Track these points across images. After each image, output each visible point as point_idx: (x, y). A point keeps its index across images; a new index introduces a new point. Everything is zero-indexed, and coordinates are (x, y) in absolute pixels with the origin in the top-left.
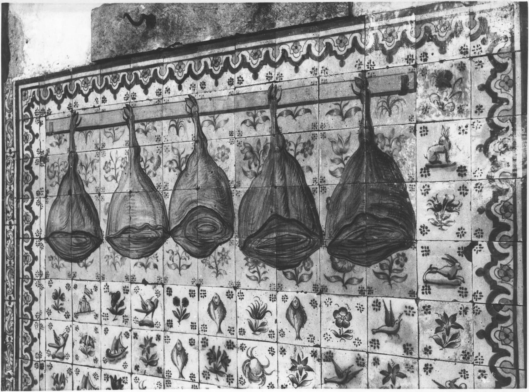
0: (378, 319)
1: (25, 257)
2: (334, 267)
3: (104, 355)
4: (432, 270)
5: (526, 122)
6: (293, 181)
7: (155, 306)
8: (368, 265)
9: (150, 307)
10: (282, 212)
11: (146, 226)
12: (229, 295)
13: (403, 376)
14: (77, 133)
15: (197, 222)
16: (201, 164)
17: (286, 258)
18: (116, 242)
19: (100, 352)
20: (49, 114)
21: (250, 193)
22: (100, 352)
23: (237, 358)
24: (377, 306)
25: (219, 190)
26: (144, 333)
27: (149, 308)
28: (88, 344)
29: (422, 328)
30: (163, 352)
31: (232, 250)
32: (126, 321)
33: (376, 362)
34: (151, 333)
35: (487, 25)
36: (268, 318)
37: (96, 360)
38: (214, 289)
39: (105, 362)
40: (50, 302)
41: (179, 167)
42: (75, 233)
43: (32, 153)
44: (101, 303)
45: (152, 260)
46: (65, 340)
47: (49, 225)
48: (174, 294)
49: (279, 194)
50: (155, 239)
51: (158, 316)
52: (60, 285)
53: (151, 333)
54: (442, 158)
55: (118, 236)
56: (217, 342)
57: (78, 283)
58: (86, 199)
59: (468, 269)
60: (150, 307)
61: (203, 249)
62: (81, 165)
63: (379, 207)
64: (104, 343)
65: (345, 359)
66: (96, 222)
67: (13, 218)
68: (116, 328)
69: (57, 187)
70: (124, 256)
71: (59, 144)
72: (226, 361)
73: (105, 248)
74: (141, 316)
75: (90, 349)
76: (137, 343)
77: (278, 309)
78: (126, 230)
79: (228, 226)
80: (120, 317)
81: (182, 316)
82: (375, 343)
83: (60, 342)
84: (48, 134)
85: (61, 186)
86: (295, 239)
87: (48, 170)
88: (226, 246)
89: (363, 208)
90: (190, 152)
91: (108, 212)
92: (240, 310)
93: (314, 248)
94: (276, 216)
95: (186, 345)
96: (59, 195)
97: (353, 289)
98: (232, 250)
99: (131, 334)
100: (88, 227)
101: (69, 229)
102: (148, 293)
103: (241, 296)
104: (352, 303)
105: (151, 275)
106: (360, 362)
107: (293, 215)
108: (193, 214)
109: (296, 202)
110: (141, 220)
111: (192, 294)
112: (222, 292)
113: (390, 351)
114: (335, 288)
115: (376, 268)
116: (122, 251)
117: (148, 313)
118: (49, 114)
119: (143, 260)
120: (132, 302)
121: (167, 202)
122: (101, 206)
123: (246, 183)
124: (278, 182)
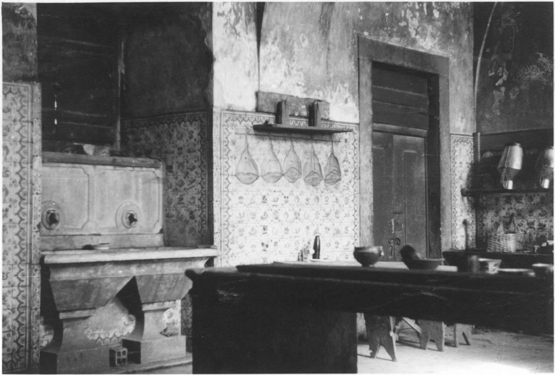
0: (334, 199)
1: (225, 183)
2: (325, 186)
3: (260, 218)
4: (344, 186)
5: (3, 321)
6: (316, 162)
7: (278, 199)
8: (332, 185)
9: (276, 200)
10: (313, 170)
11: (276, 172)
12: (300, 194)
13: (324, 217)
14: (248, 136)
15: (292, 172)
16: (292, 153)
17: (314, 184)
18: (265, 177)
19: (258, 217)
20: (236, 126)
21: (306, 163)
22: (258, 217)
23: (302, 213)
24: (334, 195)
25: (298, 162)
26: (275, 208)
27: (276, 200)
28: (254, 215)
29: (342, 201)
30: (281, 216)
31: (301, 181)
32: (268, 205)
33: (334, 210)
34: (276, 209)
35: (164, 237)
36: (310, 201)
37: (257, 221)
38: (296, 193)
39: (260, 220)
40: (238, 200)
41: (286, 153)
42: (248, 174)
43: (19, 333)
44: (259, 199)
45: (277, 183)
46: (244, 214)
47: (237, 170)
48: (284, 195)
49: (313, 164)
50: (278, 177)
51: (279, 203)
52: (241, 194)
53: (276, 209)
54: (346, 159)
55: (265, 175)
56: (297, 209)
57: (250, 193)
58: (252, 161)
59: (350, 186)
60: (276, 200)
61: (293, 180)
62: (250, 148)
63: (335, 170)
64: (261, 214)
65: (327, 210)
66: (256, 169)
67: (218, 166)
68: (264, 208)
69: (240, 156)
70: (268, 182)
71: (240, 138)
72: (299, 215)
73: (260, 179)
74: (274, 203)
75: (254, 216)
76: (271, 212)
77: (313, 198)
78: (268, 173)
79: (300, 173)
80: (266, 204)
81: (287, 202)
82: (334, 205)
83: (241, 216)
84: (236, 134)
85: (242, 155)
86: (317, 178)
87: (236, 148)
88: (300, 179)
89: (331, 170)
90: (289, 149)
91: (261, 166)
92: (303, 199)
93: (321, 180)
94: (313, 171)
95: (288, 211)
96: (241, 159)
97: (329, 191)
98: (301, 181)
99: (270, 210)
100: (254, 172)
101: (246, 172)
102: (276, 195)
103: (304, 194)
104: (329, 195)
105: (276, 189)
106: (331, 210)
107: (316, 171)
108: (290, 169)
109: (317, 167)
110: (273, 170)
111: (290, 194)
112: (298, 194)
113: (337, 207)
114: (325, 191)
115: (334, 186)
116: (267, 181)
117: (275, 202)
118: (236, 126)
119: (274, 184)
120: (270, 199)
121: (282, 164)
122: (258, 164)
123: (305, 161)
124: (313, 161)
